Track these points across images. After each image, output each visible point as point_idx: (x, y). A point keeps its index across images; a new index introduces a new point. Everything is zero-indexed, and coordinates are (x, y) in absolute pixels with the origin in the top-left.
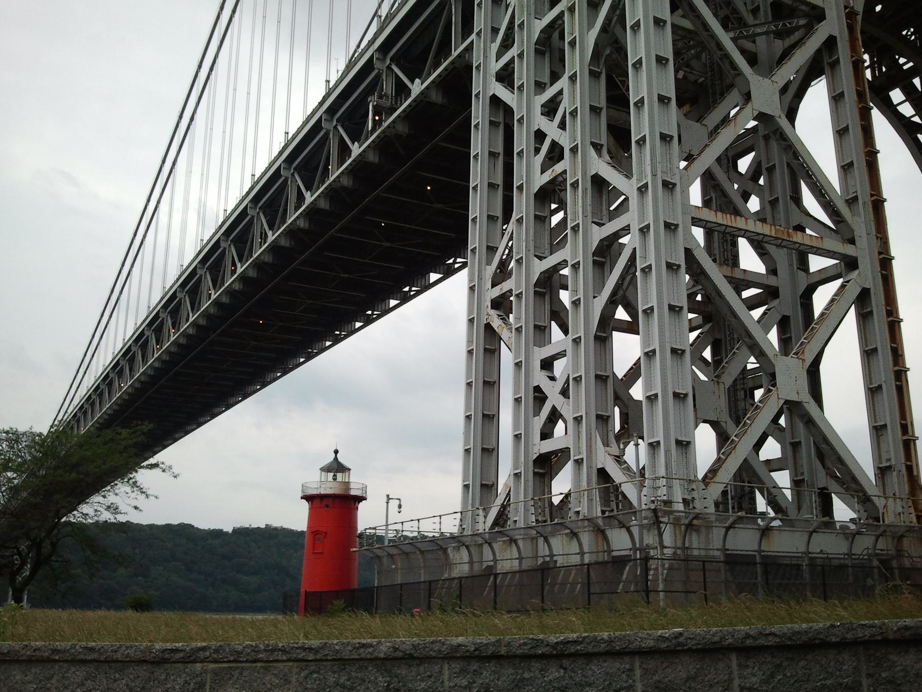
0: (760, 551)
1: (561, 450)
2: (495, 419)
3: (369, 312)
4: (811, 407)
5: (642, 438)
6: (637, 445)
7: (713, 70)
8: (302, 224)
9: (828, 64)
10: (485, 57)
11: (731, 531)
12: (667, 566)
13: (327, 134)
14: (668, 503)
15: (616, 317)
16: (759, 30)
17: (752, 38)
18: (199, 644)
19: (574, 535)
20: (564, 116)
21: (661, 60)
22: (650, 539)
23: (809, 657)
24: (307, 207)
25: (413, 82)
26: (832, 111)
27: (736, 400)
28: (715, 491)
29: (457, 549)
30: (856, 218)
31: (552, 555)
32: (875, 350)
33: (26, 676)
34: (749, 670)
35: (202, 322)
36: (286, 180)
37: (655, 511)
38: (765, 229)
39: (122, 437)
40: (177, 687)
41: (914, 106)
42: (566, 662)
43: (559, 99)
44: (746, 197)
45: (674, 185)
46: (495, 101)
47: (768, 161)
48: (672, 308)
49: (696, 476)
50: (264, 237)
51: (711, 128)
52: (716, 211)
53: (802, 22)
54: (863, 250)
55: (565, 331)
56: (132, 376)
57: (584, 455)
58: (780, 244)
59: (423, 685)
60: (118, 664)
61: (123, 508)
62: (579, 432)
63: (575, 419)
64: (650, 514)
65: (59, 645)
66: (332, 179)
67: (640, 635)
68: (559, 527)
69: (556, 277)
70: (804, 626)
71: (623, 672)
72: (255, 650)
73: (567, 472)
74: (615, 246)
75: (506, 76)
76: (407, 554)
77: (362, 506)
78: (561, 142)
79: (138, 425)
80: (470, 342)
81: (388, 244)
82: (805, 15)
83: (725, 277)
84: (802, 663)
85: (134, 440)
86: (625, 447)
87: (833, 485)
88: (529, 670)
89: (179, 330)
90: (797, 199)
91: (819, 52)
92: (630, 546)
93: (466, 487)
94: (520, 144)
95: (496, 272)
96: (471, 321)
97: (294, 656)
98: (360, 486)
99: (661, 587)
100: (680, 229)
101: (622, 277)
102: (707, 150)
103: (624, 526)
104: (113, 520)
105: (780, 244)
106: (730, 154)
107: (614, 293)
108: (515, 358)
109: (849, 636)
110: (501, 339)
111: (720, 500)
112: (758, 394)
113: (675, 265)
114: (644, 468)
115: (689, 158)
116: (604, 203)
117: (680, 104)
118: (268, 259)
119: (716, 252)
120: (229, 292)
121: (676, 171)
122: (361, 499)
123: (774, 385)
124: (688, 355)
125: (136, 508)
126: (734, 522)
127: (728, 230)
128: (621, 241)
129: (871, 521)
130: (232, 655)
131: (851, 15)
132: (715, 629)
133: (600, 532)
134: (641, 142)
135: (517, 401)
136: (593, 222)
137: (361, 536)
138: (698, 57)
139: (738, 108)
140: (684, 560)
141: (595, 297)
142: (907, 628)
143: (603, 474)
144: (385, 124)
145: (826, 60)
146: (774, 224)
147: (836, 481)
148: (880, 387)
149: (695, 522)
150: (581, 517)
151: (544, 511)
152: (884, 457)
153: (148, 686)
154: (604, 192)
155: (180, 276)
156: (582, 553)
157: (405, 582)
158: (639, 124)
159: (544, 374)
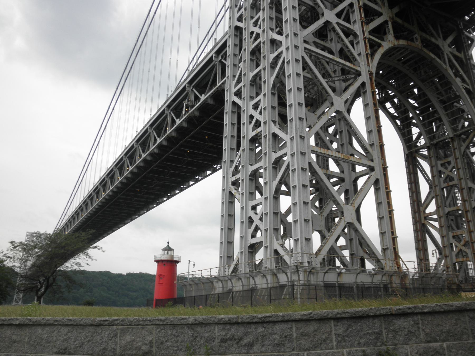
0: (337, 282)
1: (260, 242)
2: (233, 230)
3: (182, 187)
4: (357, 225)
5: (292, 237)
6: (290, 240)
7: (319, 93)
8: (156, 151)
9: (363, 92)
10: (230, 86)
11: (326, 274)
12: (301, 288)
13: (166, 116)
14: (302, 263)
15: (282, 189)
16: (336, 79)
17: (334, 82)
18: (115, 318)
19: (264, 276)
20: (261, 110)
21: (299, 89)
22: (295, 277)
23: (362, 321)
24: (158, 144)
25: (201, 95)
26: (364, 110)
27: (328, 222)
28: (320, 258)
29: (217, 282)
30: (374, 151)
31: (255, 284)
32: (381, 203)
33: (43, 331)
34: (338, 327)
35: (115, 190)
36: (150, 133)
37: (297, 266)
38: (339, 155)
39: (83, 235)
40: (106, 335)
41: (395, 109)
42: (265, 325)
43: (259, 103)
44: (332, 142)
45: (304, 137)
46: (234, 103)
47: (340, 129)
48: (304, 186)
49: (313, 252)
50: (140, 156)
51: (318, 115)
52: (320, 148)
53: (353, 76)
54: (376, 164)
55: (261, 194)
56: (86, 211)
57: (268, 244)
58: (345, 161)
59: (207, 335)
60: (81, 326)
61: (82, 264)
62: (267, 235)
63: (265, 230)
64: (295, 268)
65: (57, 318)
66: (168, 133)
67: (295, 314)
68: (258, 273)
69: (258, 173)
70: (360, 309)
71: (288, 329)
72: (139, 321)
73: (262, 250)
74: (281, 161)
75: (238, 94)
76: (197, 284)
77: (178, 265)
78: (260, 120)
79: (89, 231)
80: (223, 198)
81: (190, 159)
82: (354, 74)
83: (324, 174)
84: (359, 324)
85: (88, 237)
86: (285, 241)
87: (365, 256)
88: (250, 328)
89: (105, 193)
90: (351, 144)
91: (359, 88)
92: (287, 280)
93: (221, 257)
94: (244, 120)
95: (233, 171)
96: (223, 190)
97: (154, 323)
98: (178, 257)
99: (299, 296)
100: (307, 155)
101: (284, 173)
102: (317, 124)
103: (284, 272)
104: (78, 269)
105: (345, 161)
106: (326, 126)
107: (281, 179)
108: (241, 205)
109: (378, 313)
110: (235, 197)
111: (322, 262)
112: (337, 220)
113: (305, 169)
114: (292, 249)
115: (310, 127)
116: (277, 144)
117: (306, 106)
118: (142, 165)
119: (320, 164)
120: (126, 178)
121: (305, 132)
122: (178, 262)
123: (343, 216)
124: (310, 204)
125: (88, 264)
126: (328, 271)
127: (325, 155)
128: (283, 159)
129: (380, 269)
130: (129, 322)
131: (371, 74)
132: (325, 311)
133: (275, 275)
134: (291, 120)
135: (242, 222)
136: (273, 151)
137: (178, 276)
138: (313, 88)
139: (328, 108)
140: (308, 286)
141: (273, 181)
142: (400, 309)
143: (276, 252)
144: (190, 112)
145: (362, 91)
146: (342, 153)
147: (367, 254)
148: (383, 217)
149: (312, 271)
150: (267, 269)
151: (252, 267)
152: (385, 244)
153: (94, 335)
154: (277, 140)
155: (107, 171)
156: (267, 283)
157: (196, 295)
158: (290, 113)
159: (253, 211)
